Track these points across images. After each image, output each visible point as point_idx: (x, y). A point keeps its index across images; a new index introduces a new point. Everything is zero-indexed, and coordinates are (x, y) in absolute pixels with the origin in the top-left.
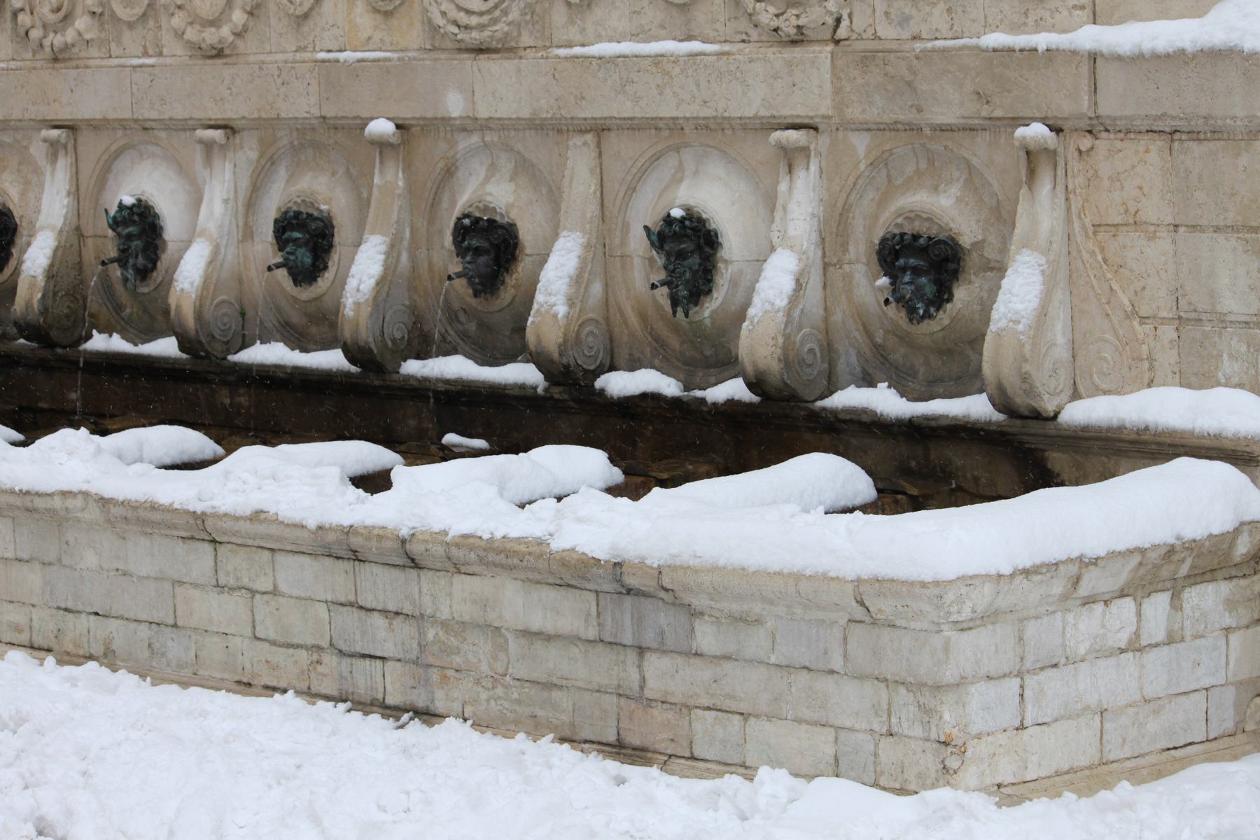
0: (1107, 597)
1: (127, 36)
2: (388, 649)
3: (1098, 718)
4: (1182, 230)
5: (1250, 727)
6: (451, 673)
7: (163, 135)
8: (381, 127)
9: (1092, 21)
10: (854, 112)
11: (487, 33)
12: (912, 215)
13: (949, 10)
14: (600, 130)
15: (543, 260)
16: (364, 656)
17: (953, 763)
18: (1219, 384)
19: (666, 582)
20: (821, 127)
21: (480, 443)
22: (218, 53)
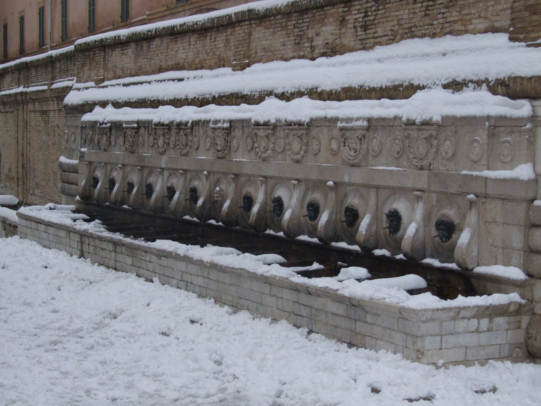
0: (469, 318)
1: (279, 156)
2: (304, 315)
3: (465, 349)
4: (505, 224)
5: (514, 356)
6: (316, 321)
7: (285, 181)
8: (330, 183)
9: (74, 197)
10: (432, 188)
11: (354, 162)
12: (444, 215)
13: (455, 164)
14: (378, 188)
15: (362, 220)
16: (299, 315)
17: (420, 356)
18: (511, 265)
19: (360, 304)
20: (426, 191)
21: (345, 264)
22: (298, 162)
